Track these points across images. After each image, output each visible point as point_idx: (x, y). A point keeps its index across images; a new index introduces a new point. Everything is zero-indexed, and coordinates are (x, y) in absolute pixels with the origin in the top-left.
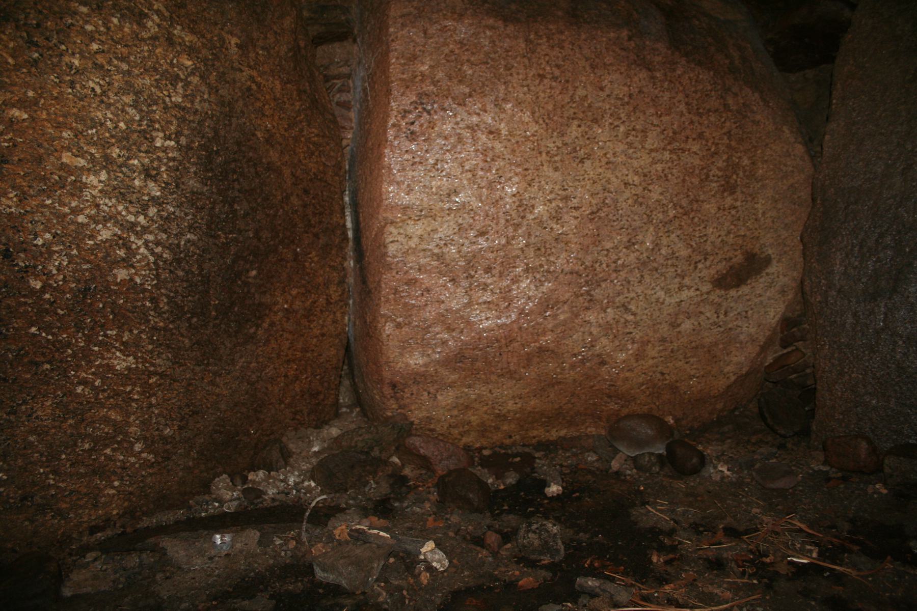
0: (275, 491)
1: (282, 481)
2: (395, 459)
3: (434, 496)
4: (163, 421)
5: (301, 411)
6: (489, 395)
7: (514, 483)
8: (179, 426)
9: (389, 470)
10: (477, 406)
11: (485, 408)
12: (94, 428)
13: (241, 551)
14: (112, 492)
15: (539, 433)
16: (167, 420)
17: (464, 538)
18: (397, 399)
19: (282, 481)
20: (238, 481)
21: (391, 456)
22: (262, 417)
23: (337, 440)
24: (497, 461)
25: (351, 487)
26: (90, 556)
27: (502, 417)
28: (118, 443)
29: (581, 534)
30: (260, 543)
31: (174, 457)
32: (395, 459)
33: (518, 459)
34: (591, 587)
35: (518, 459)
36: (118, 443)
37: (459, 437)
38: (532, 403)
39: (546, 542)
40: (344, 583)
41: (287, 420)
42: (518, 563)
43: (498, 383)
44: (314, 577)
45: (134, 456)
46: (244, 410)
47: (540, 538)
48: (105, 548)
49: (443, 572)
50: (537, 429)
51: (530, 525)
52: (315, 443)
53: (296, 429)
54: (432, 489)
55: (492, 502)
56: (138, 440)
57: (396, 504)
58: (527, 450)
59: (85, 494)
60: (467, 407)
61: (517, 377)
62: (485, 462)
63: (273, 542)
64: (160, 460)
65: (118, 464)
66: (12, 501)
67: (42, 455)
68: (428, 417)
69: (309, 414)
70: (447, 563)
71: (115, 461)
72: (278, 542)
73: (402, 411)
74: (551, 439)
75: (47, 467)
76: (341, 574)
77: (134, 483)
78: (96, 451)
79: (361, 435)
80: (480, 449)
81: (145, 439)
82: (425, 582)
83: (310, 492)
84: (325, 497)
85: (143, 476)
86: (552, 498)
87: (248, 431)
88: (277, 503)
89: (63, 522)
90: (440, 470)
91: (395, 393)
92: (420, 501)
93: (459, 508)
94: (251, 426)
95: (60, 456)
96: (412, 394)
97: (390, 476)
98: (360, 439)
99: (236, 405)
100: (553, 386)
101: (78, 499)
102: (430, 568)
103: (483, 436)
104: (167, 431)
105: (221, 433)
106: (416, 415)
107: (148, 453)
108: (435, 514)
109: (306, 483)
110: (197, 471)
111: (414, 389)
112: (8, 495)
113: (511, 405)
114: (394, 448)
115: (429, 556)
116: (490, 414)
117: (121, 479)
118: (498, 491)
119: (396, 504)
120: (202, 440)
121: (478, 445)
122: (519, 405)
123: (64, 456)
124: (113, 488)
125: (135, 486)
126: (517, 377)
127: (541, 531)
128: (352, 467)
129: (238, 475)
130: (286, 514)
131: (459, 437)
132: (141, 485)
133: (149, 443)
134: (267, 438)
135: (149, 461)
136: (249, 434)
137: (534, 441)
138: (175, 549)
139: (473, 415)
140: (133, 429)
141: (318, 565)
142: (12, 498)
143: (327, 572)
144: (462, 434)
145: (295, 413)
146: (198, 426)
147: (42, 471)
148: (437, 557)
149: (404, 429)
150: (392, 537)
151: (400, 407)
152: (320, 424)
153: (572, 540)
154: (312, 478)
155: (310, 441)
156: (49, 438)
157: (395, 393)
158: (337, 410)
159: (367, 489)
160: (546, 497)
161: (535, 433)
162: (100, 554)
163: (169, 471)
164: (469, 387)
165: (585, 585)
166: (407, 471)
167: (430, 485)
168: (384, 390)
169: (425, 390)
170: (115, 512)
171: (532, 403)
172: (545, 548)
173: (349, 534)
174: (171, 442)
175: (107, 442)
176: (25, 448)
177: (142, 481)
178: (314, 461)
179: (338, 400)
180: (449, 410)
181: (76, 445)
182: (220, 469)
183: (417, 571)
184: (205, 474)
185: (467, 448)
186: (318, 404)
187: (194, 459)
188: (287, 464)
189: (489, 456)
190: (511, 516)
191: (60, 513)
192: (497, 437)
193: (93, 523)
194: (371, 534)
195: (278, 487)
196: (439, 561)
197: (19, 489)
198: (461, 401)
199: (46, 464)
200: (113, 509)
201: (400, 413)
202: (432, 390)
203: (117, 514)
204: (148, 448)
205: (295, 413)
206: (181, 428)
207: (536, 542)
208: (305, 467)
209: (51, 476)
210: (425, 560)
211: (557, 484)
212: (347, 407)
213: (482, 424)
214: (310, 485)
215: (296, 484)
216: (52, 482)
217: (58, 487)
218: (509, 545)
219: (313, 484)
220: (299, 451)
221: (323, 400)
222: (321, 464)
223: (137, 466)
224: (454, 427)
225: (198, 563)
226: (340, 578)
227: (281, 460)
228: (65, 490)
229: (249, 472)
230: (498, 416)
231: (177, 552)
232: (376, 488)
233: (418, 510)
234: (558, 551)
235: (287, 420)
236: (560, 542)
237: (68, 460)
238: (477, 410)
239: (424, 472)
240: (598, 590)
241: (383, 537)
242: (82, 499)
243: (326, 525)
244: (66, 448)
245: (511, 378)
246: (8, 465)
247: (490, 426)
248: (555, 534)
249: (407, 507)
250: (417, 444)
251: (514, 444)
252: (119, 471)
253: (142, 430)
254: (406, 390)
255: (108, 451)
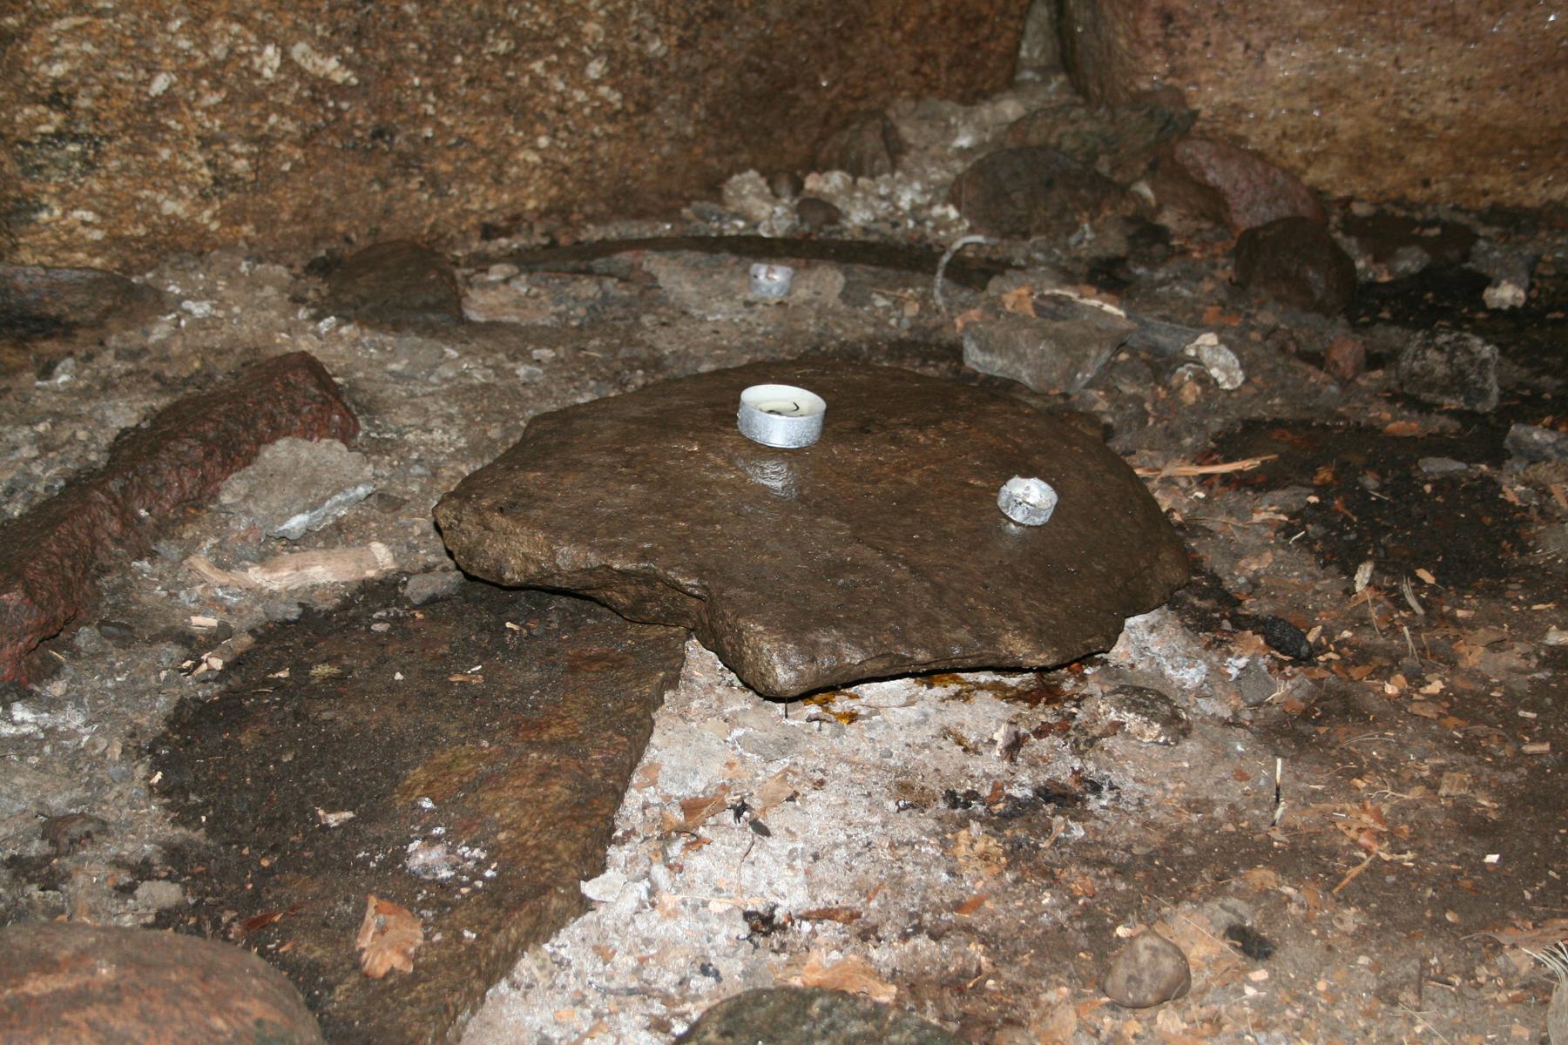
0: (868, 215)
1: (882, 198)
2: (1145, 190)
3: (1227, 271)
4: (650, 21)
5: (935, 56)
6: (1391, 69)
7: (1414, 269)
8: (680, 38)
9: (1130, 208)
10: (1358, 93)
11: (1378, 100)
12: (521, 11)
13: (809, 303)
14: (533, 158)
15: (1498, 184)
16: (658, 20)
17: (1283, 349)
18: (1169, 52)
19: (882, 198)
20: (785, 188)
21: (1136, 180)
22: (850, 53)
23: (1014, 126)
24: (1385, 231)
25: (1038, 230)
26: (496, 273)
27: (1414, 131)
28: (560, 52)
29: (1544, 379)
30: (844, 296)
31: (659, 109)
32: (1145, 190)
33: (1436, 231)
34: (1536, 443)
35: (1436, 231)
36: (560, 52)
37: (1301, 165)
38: (1495, 104)
39: (1462, 373)
40: (1025, 376)
41: (901, 72)
42: (1391, 400)
43: (1419, 43)
44: (961, 362)
45: (584, 87)
46: (816, 29)
47: (1450, 361)
48: (525, 261)
49: (1228, 392)
50: (1496, 174)
51: (1433, 335)
52: (962, 130)
53: (917, 98)
54: (1222, 261)
55: (1358, 303)
56: (596, 53)
57: (1140, 271)
58: (1461, 218)
59: (483, 151)
60: (1334, 94)
61: (1470, 33)
62: (1352, 226)
63: (870, 301)
64: (631, 108)
65: (553, 99)
66: (358, 133)
67: (421, 48)
68: (1234, 106)
69: (949, 68)
70: (1240, 377)
71: (547, 91)
72: (881, 302)
73: (1177, 82)
74: (1528, 203)
75: (428, 75)
76: (1021, 357)
77: (576, 149)
78: (516, 61)
79: (1073, 122)
80: (1347, 202)
81: (611, 53)
82: (1192, 400)
83: (947, 228)
84: (979, 239)
85: (594, 137)
86: (1497, 312)
87: (817, 79)
88: (874, 238)
89: (436, 201)
90: (1244, 221)
91: (1168, 35)
92: (1193, 275)
93: (1279, 299)
94: (824, 69)
95: (453, 56)
96: (1207, 44)
97: (1128, 221)
98: (1072, 129)
99: (801, 13)
100: (1556, 70)
101: (471, 160)
102: (1203, 379)
103: (1361, 171)
104: (655, 47)
105: (761, 71)
106: (1208, 97)
107: (613, 87)
108: (1222, 304)
109: (937, 211)
110: (698, 150)
111: (1215, 31)
112: (354, 119)
113: (1441, 104)
114: (1143, 166)
115: (1206, 355)
116: (1387, 120)
117: (553, 135)
118: (1372, 284)
119: (1140, 271)
120: (720, 82)
121: (1341, 193)
122: (1461, 106)
123: (458, 60)
124: (536, 149)
125: (576, 156)
126: (1470, 33)
127: (1454, 349)
128: (1049, 184)
129: (784, 175)
130: (898, 256)
131: (1301, 165)
132: (587, 155)
133: (617, 65)
134: (850, 106)
135: (610, 104)
136: (816, 88)
137: (1485, 203)
138: (675, 278)
139: (1346, 116)
140: (591, 27)
141: (973, 338)
142: (358, 127)
143: (991, 351)
144: (1309, 160)
145: (922, 59)
146: (717, 46)
147: (417, 81)
148: (1221, 359)
149: (1174, 121)
150: (1129, 317)
151: (1172, 72)
152: (972, 96)
153: (1521, 386)
154: (954, 199)
155: (948, 127)
156: (439, 13)
157: (1168, 35)
158: (1014, 71)
159: (1073, 240)
160: (1482, 306)
161: (1489, 182)
162: (516, 270)
163: (644, 137)
164: (1348, 43)
165: (1525, 438)
166: (1168, 219)
167: (1218, 251)
168: (1142, 24)
169: (1240, 38)
170: (531, 204)
171: (1495, 104)
172: (1458, 382)
173: (1036, 306)
174: (658, 73)
175: (539, 45)
176: (395, 27)
177: (591, 148)
178: (959, 166)
179: (1018, 47)
180: (1287, 94)
181: (483, 38)
182: (745, 157)
183: (1175, 382)
184: (714, 161)
185: (1316, 193)
186: (974, 47)
187: (698, 122)
188: (894, 166)
189: (1367, 218)
190: (1393, 330)
191: (434, 182)
192: (1392, 179)
193: (487, 219)
194: (1084, 306)
195: (872, 208)
196: (1225, 369)
197: (374, 112)
198: (1320, 77)
199: (426, 69)
200: (529, 197)
201: (1170, 88)
202: (1256, 40)
203: (536, 209)
204: (614, 76)
205: (922, 59)
206: (683, 44)
207: (1441, 370)
208: (937, 175)
209: (431, 97)
210: (1196, 360)
211: (1518, 284)
212: (1038, 70)
213: (1362, 141)
214: (946, 216)
215: (915, 209)
216: (431, 110)
217: (439, 125)
218: (1379, 374)
219: (953, 213)
220: (922, 144)
221: (987, 39)
222: (979, 170)
223: (587, 111)
224: (1293, 140)
225: (720, 312)
226: (1017, 365)
227: (884, 154)
228: (450, 134)
229: (807, 173)
230: (1405, 125)
231: (679, 283)
232: (1092, 237)
233: (1186, 293)
234: (1483, 394)
235: (901, 72)
236: (1492, 378)
237: (465, 69)
238: (1356, 103)
239: (1206, 225)
240: (1549, 451)
241: (1107, 314)
242: (477, 159)
243: (984, 288)
244: (466, 42)
245: (1454, 34)
246: (363, 55)
247: (1381, 149)
248: (1485, 362)
249: (1162, 283)
250: (1202, 159)
251: (1434, 200)
252: (551, 115)
253: (608, 34)
254: (1195, 32)
255: (538, 66)
